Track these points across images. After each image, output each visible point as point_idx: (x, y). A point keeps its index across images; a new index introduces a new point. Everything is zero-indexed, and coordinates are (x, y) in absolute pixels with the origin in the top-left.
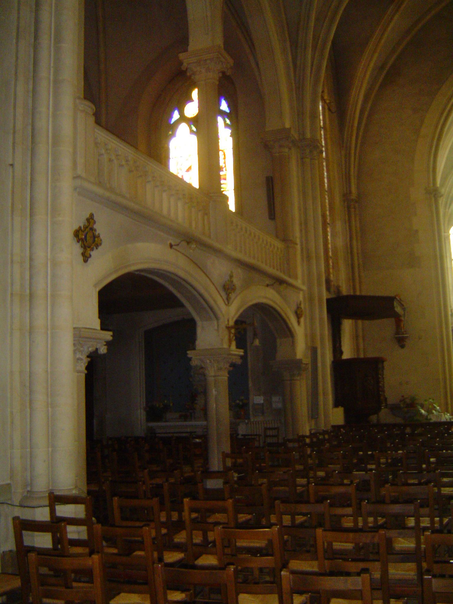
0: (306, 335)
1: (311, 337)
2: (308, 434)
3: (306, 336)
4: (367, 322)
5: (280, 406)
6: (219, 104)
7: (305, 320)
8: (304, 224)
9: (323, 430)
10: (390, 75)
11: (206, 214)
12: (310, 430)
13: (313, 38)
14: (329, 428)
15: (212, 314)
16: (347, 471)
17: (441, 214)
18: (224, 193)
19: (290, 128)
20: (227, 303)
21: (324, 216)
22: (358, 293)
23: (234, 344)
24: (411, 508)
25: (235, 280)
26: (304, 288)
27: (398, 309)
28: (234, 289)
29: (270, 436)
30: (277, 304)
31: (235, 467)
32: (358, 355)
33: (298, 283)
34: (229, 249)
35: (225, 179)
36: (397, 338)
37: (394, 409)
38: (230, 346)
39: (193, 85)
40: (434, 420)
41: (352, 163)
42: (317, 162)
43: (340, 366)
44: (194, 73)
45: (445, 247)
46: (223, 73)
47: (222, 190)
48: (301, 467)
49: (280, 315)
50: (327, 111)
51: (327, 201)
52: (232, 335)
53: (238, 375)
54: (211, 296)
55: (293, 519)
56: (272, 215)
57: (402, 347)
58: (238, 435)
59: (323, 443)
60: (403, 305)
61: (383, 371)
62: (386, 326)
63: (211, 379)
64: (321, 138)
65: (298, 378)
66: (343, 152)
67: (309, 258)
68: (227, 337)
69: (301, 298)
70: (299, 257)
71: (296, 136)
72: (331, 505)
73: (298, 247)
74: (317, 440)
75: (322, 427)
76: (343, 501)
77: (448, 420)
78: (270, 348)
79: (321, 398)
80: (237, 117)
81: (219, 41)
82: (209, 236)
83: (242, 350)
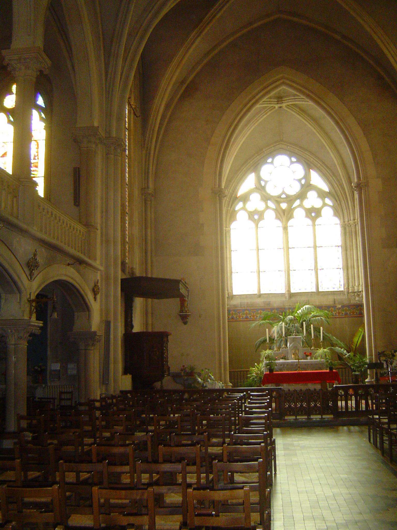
0: (101, 310)
1: (105, 312)
2: (98, 398)
3: (101, 311)
4: (156, 301)
5: (75, 372)
6: (36, 99)
7: (101, 296)
8: (105, 211)
9: (112, 395)
10: (188, 90)
11: (16, 197)
12: (101, 395)
13: (125, 51)
14: (118, 393)
15: (15, 289)
16: (129, 432)
17: (224, 212)
18: (34, 179)
19: (98, 127)
20: (30, 279)
21: (123, 206)
22: (149, 276)
23: (34, 316)
24: (179, 466)
25: (39, 259)
26: (102, 268)
27: (183, 291)
28: (37, 266)
29: (64, 399)
30: (75, 281)
31: (30, 428)
32: (147, 328)
33: (97, 264)
34: (34, 230)
35: (36, 167)
36: (180, 315)
37: (176, 376)
38: (30, 318)
39: (13, 80)
40: (209, 387)
41: (151, 161)
42: (120, 158)
43: (131, 340)
44: (14, 69)
45: (226, 240)
46: (41, 71)
47: (32, 176)
48: (90, 428)
49: (78, 290)
50: (132, 115)
51: (127, 193)
52: (33, 308)
53: (37, 344)
54: (15, 272)
55: (78, 477)
56: (77, 201)
57: (185, 323)
58: (35, 398)
59: (112, 406)
60: (187, 288)
61: (167, 344)
62: (170, 305)
63: (12, 347)
64: (125, 138)
65: (93, 348)
66: (144, 152)
67: (107, 241)
68: (28, 310)
69: (99, 278)
70: (99, 241)
71: (103, 135)
72: (110, 464)
73: (99, 232)
74: (107, 404)
75: (112, 392)
76: (123, 460)
77: (221, 388)
78: (68, 320)
79: (112, 366)
80: (52, 111)
81: (40, 43)
82: (17, 217)
83: (41, 322)
